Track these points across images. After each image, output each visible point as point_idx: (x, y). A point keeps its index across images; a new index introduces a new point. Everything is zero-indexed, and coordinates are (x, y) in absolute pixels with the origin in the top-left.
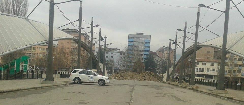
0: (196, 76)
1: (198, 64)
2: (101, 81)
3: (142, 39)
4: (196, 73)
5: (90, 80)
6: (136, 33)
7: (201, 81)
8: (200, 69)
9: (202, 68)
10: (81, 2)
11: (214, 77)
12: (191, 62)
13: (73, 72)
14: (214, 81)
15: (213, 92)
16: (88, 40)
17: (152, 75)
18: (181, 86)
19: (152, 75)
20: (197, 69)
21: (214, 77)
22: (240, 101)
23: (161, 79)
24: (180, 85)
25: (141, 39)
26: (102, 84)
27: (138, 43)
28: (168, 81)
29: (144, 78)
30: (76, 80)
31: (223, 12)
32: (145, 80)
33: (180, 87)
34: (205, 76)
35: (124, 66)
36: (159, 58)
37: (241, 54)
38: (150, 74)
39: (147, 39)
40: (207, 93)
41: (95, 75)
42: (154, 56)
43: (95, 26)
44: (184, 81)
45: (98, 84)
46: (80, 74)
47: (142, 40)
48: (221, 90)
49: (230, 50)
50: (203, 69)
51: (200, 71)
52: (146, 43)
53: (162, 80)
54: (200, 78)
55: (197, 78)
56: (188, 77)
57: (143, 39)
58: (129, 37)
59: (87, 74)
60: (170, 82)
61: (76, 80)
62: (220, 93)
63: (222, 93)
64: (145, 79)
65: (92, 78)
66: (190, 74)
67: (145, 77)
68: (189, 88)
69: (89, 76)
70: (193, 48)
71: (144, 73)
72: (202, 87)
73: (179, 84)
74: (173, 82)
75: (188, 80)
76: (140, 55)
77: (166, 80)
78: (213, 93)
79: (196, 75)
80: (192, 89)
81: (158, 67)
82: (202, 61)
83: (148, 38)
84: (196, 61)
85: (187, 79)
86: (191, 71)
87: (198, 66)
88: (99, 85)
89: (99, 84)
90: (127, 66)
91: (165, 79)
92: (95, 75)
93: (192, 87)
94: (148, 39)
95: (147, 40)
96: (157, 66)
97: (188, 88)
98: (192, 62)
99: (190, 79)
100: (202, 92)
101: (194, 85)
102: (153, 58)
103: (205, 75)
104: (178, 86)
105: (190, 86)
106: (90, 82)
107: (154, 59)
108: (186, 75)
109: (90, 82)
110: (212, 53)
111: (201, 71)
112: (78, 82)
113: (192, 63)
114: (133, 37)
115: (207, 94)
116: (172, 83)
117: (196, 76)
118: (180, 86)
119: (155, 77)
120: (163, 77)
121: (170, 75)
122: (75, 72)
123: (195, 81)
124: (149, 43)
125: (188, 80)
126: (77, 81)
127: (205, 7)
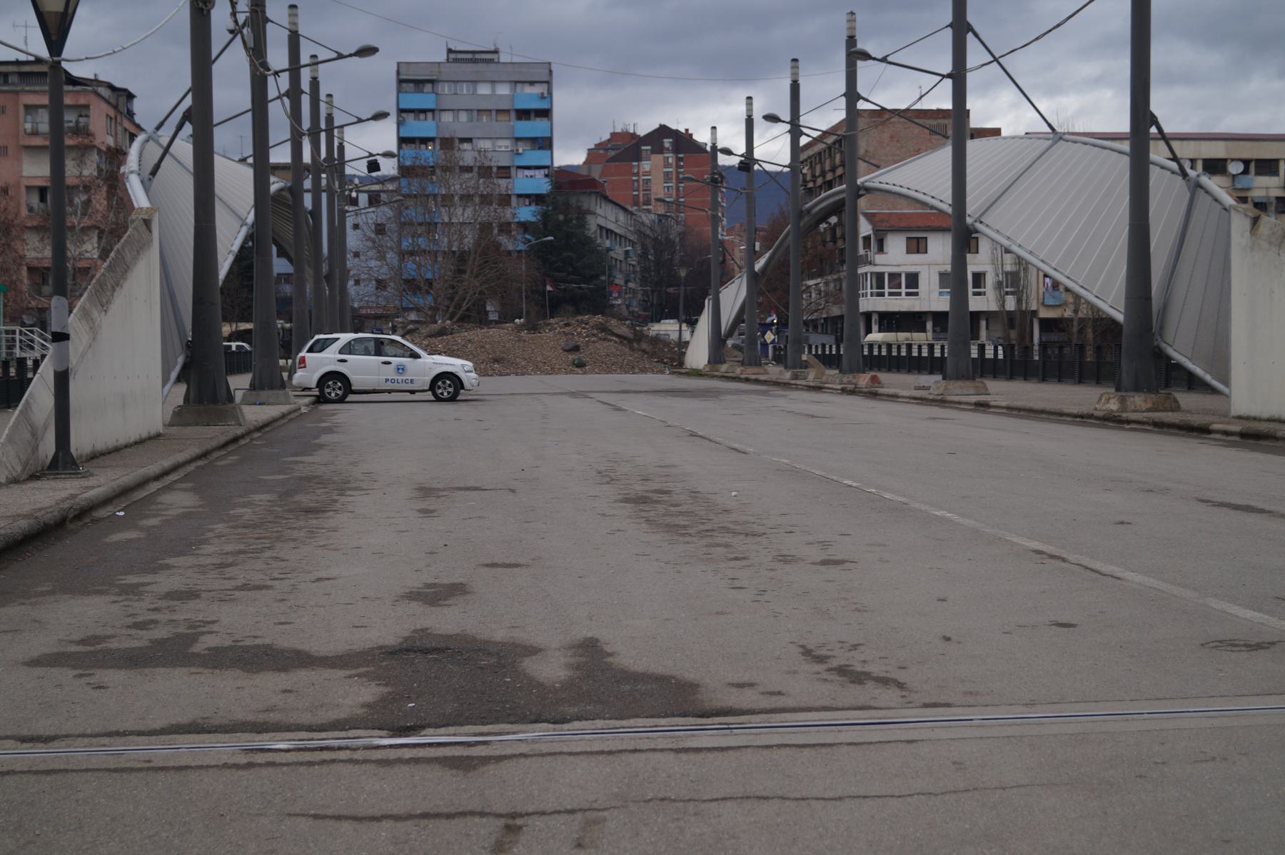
0: (875, 327)
1: (881, 249)
2: (444, 383)
3: (493, 90)
4: (869, 303)
5: (393, 381)
6: (450, 51)
7: (880, 351)
8: (894, 277)
9: (912, 269)
10: (294, 11)
11: (983, 323)
12: (834, 240)
13: (310, 350)
14: (982, 348)
15: (934, 393)
16: (127, 124)
18: (803, 382)
20: (880, 276)
21: (983, 323)
22: (1008, 408)
23: (673, 356)
24: (796, 377)
25: (484, 90)
26: (449, 393)
28: (724, 368)
29: (571, 357)
30: (329, 386)
31: (944, 76)
32: (578, 370)
33: (797, 387)
34: (929, 325)
35: (381, 284)
36: (622, 216)
37: (1015, 243)
38: (603, 328)
39: (529, 90)
40: (910, 398)
43: (351, 55)
44: (814, 361)
45: (429, 396)
47: (493, 94)
48: (960, 383)
49: (981, 222)
50: (913, 280)
51: (899, 294)
52: (524, 114)
53: (681, 364)
54: (902, 336)
55: (882, 335)
56: (825, 332)
58: (401, 82)
59: (378, 353)
61: (329, 386)
62: (959, 392)
63: (966, 392)
64: (580, 365)
65: (401, 369)
66: (836, 311)
67: (576, 349)
68: (839, 387)
69: (389, 363)
70: (841, 196)
71: (567, 329)
72: (892, 381)
73: (787, 375)
74: (755, 370)
75: (831, 351)
76: (505, 200)
77: (709, 362)
78: (931, 397)
79: (875, 318)
80: (854, 392)
82: (903, 224)
83: (532, 83)
84: (865, 228)
85: (824, 346)
86: (844, 296)
87: (879, 258)
88: (439, 399)
89: (435, 394)
90: (412, 285)
91: (698, 354)
92: (415, 356)
93: (854, 381)
94: (537, 90)
95: (529, 97)
97: (835, 386)
98: (843, 237)
99: (838, 349)
100: (894, 397)
101: (756, 365)
102: (582, 214)
103: (930, 317)
104: (785, 384)
105: (845, 380)
106: (390, 392)
107: (593, 223)
108: (813, 325)
109: (390, 392)
111: (903, 290)
112: (337, 395)
113: (840, 244)
114: (432, 82)
115: (912, 401)
116: (750, 372)
117: (875, 327)
118: (798, 382)
119: (635, 344)
121: (730, 334)
122: (320, 347)
123: (866, 353)
125: (831, 351)
126: (334, 389)
127: (875, 59)
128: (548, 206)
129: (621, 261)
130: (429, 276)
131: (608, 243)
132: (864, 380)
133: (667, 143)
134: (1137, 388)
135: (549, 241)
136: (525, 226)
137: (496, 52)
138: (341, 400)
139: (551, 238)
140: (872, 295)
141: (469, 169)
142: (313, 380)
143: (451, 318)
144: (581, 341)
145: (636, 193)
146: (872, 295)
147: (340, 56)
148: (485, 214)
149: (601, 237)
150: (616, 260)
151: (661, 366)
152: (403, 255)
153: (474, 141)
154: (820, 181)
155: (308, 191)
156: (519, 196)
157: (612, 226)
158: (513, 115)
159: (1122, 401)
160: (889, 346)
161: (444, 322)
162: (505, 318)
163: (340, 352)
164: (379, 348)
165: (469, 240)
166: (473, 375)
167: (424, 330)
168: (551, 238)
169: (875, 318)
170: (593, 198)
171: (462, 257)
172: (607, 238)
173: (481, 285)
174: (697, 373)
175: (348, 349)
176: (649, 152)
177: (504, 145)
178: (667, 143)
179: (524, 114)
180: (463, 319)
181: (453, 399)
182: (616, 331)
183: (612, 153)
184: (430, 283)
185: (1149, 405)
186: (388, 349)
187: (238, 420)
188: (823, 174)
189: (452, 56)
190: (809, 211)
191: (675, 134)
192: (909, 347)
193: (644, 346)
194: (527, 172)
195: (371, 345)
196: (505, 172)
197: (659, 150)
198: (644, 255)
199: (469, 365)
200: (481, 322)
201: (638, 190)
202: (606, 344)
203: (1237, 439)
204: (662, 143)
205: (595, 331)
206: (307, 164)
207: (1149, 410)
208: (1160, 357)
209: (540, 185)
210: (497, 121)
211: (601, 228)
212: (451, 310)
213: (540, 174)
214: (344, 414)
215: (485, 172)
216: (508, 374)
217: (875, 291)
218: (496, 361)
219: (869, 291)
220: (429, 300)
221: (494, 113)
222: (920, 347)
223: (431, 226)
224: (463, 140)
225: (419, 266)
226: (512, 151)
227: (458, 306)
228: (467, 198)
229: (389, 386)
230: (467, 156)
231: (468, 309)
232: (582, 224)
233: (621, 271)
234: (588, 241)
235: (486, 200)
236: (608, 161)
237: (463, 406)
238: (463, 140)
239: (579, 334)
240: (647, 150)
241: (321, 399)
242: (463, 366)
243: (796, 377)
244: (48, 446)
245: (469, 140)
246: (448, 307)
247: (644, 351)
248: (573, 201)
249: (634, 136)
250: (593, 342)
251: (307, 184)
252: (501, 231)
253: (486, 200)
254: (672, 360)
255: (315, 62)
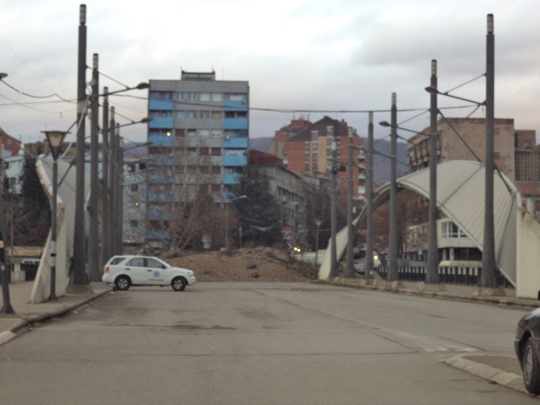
3: (211, 98)
5: (153, 280)
6: (183, 73)
13: (112, 263)
17: (279, 259)
19: (279, 259)
25: (205, 98)
27: (195, 116)
28: (337, 279)
32: (255, 279)
36: (294, 181)
38: (270, 255)
39: (233, 98)
41: (164, 267)
42: (272, 172)
45: (170, 288)
46: (128, 267)
49: (444, 206)
52: (230, 114)
53: (316, 277)
57: (218, 98)
60: (343, 280)
64: (257, 276)
65: (157, 274)
67: (254, 267)
69: (150, 271)
76: (217, 169)
79: (451, 251)
81: (291, 222)
83: (236, 94)
85: (420, 268)
88: (175, 290)
90: (154, 224)
91: (325, 272)
92: (164, 267)
94: (239, 98)
96: (285, 216)
102: (267, 179)
106: (151, 285)
107: (273, 186)
109: (151, 285)
110: (509, 157)
114: (171, 93)
117: (452, 257)
119: (289, 265)
120: (318, 266)
121: (343, 258)
122: (117, 261)
124: (244, 114)
126: (123, 284)
128: (244, 175)
129: (293, 210)
130: (167, 219)
131: (284, 199)
132: (394, 284)
133: (330, 128)
134: (487, 286)
135: (244, 199)
136: (229, 187)
137: (213, 73)
138: (126, 289)
139: (244, 197)
140: (450, 236)
141: (194, 149)
142: (113, 279)
143: (180, 246)
144: (257, 263)
145: (307, 162)
146: (450, 236)
147: (133, 123)
148: (206, 178)
149: (280, 194)
150: (290, 210)
151: (303, 278)
152: (149, 204)
153: (198, 131)
154: (420, 162)
155: (88, 162)
156: (226, 167)
157: (286, 187)
158: (223, 114)
159: (480, 291)
160: (456, 268)
161: (175, 249)
162: (215, 247)
163: (127, 265)
164: (145, 263)
165: (193, 196)
166: (193, 278)
167: (165, 254)
168: (244, 197)
169: (451, 251)
170: (274, 170)
171: (188, 208)
172: (284, 195)
173: (199, 226)
174: (323, 282)
175: (131, 263)
176: (317, 135)
177: (218, 133)
178: (330, 128)
179: (230, 114)
180: (188, 248)
181: (182, 289)
182: (279, 257)
183: (292, 135)
184: (166, 223)
185: (492, 293)
186: (150, 263)
187: (92, 292)
188: (422, 157)
189: (185, 76)
190: (378, 193)
191: (335, 123)
192: (468, 269)
193: (295, 266)
194: (232, 152)
195: (142, 262)
196: (217, 151)
197: (324, 133)
198: (308, 207)
199: (191, 272)
200: (198, 249)
201: (309, 161)
202: (272, 264)
203: (505, 305)
204: (326, 129)
205: (265, 257)
206: (88, 143)
207: (492, 295)
208: (497, 272)
209: (240, 159)
210: (213, 118)
211: (279, 188)
212: (180, 242)
213: (240, 153)
214: (133, 295)
215: (204, 151)
216: (213, 281)
217: (452, 234)
218: (207, 273)
219: (448, 234)
220: (166, 234)
221: (211, 113)
222: (473, 270)
223: (168, 185)
224: (190, 130)
225: (160, 212)
226: (222, 138)
227: (185, 239)
228: (191, 167)
229: (151, 283)
230: (192, 140)
231: (191, 241)
232: (266, 185)
233: (293, 217)
234: (269, 198)
235: (204, 169)
236: (288, 141)
237: (187, 294)
238: (190, 130)
239: (257, 258)
240: (315, 134)
241: (117, 288)
242: (188, 273)
243: (368, 284)
244: (48, 293)
245: (194, 130)
246: (178, 240)
247: (295, 269)
248: (261, 171)
249: (307, 123)
250: (264, 263)
251: (88, 157)
252: (213, 190)
253: (204, 169)
254: (312, 274)
255: (106, 95)
